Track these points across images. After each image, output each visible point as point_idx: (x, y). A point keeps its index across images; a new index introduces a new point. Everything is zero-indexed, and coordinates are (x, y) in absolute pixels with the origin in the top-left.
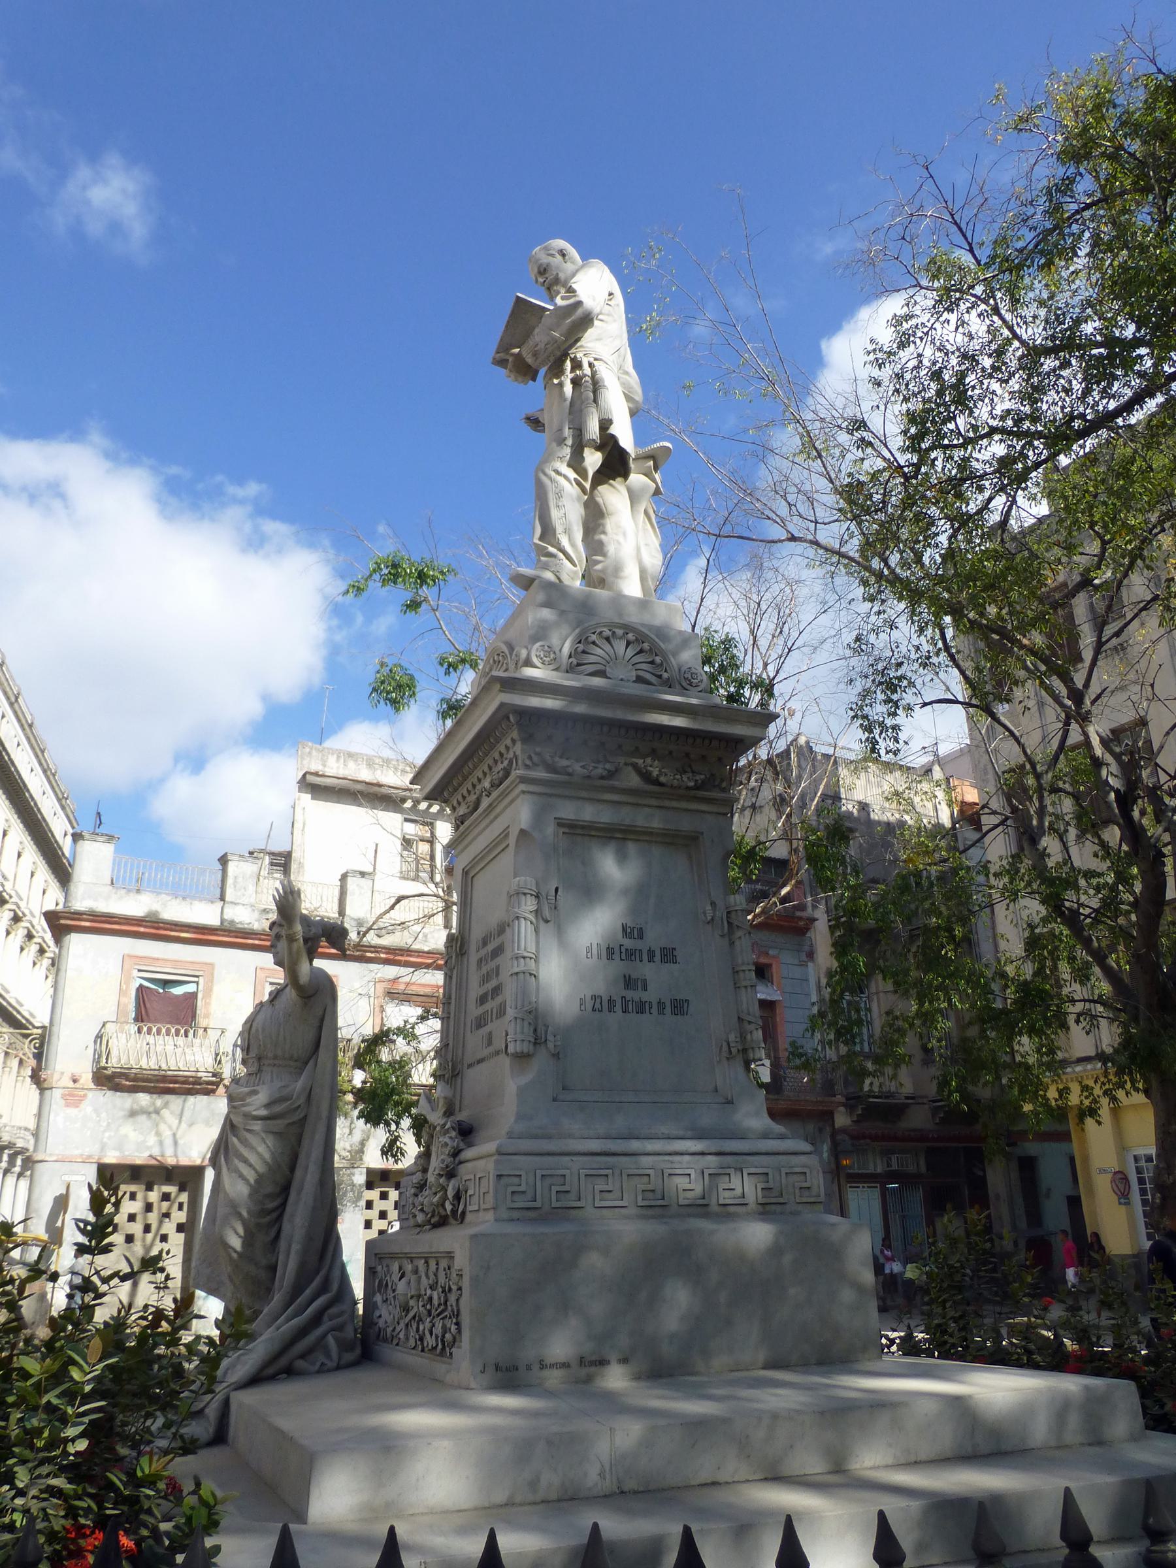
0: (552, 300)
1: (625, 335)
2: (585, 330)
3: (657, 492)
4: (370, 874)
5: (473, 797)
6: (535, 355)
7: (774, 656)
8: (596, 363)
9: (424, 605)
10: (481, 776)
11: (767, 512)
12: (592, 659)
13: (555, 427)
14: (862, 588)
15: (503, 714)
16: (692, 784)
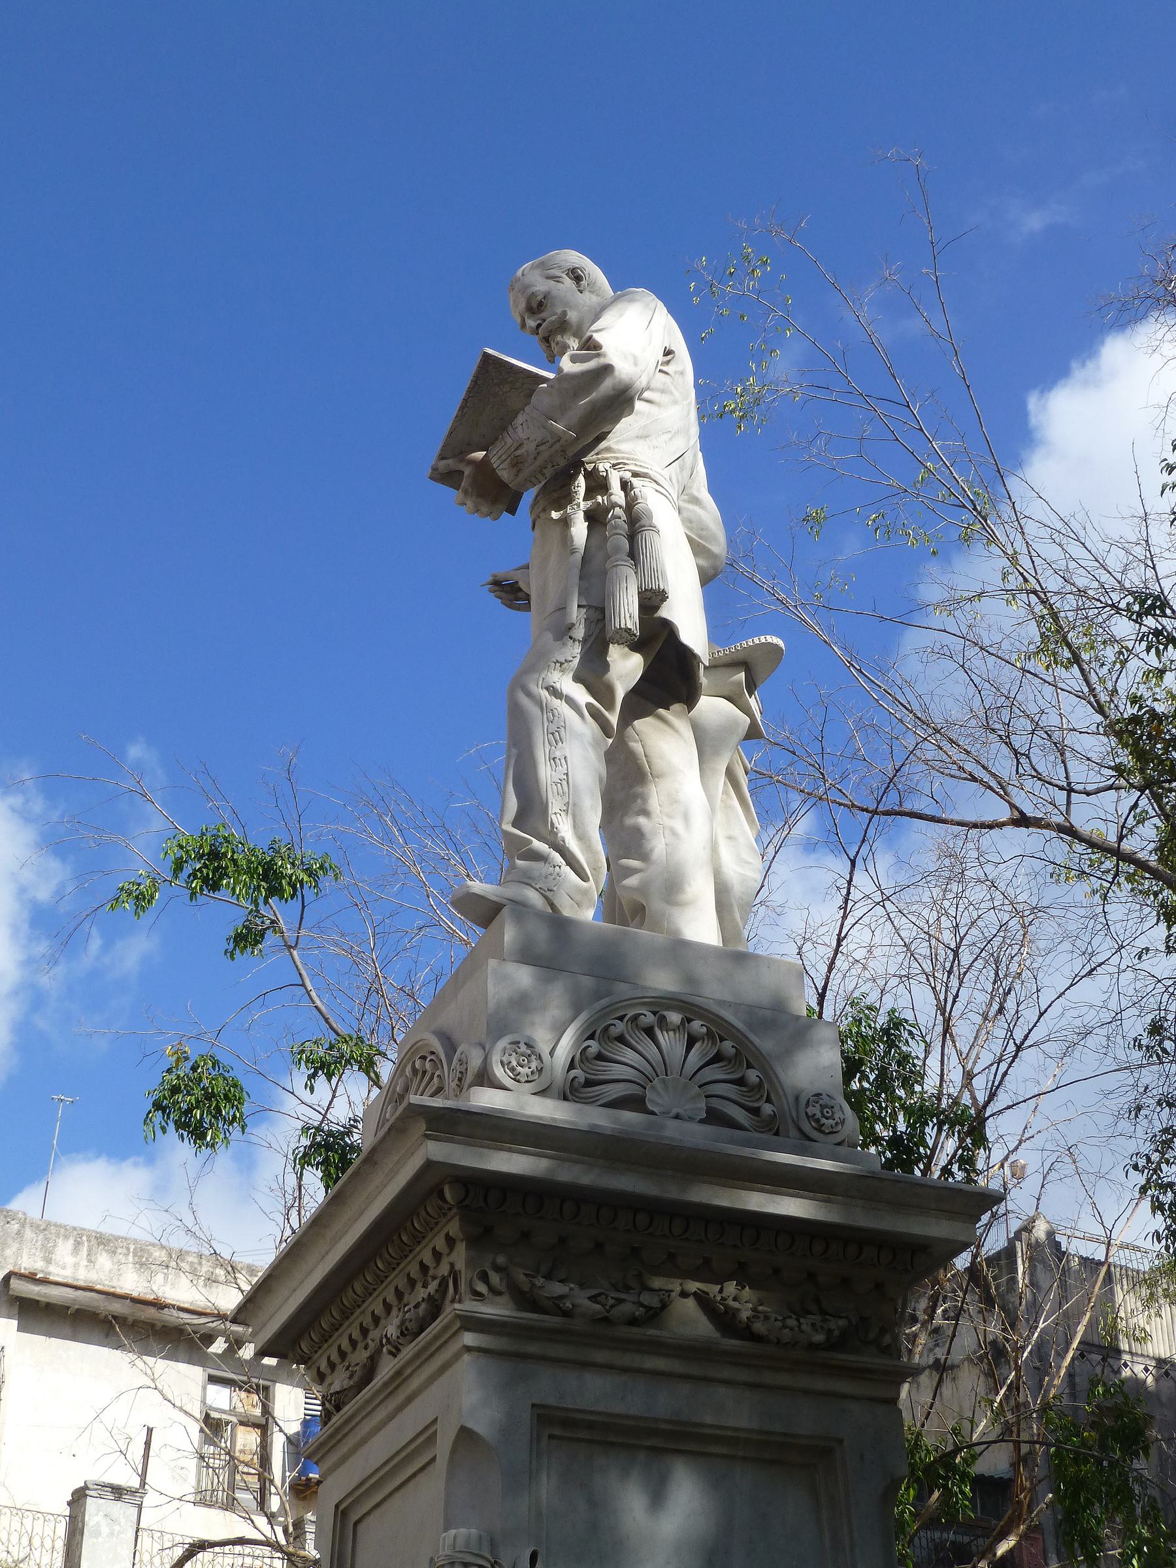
0: (552, 360)
1: (695, 430)
2: (617, 420)
3: (753, 733)
4: (133, 1492)
5: (361, 1356)
6: (517, 464)
7: (986, 1058)
8: (636, 482)
9: (271, 939)
10: (379, 1309)
11: (970, 766)
12: (617, 1071)
13: (552, 603)
14: (1163, 926)
15: (433, 1183)
16: (819, 1338)
